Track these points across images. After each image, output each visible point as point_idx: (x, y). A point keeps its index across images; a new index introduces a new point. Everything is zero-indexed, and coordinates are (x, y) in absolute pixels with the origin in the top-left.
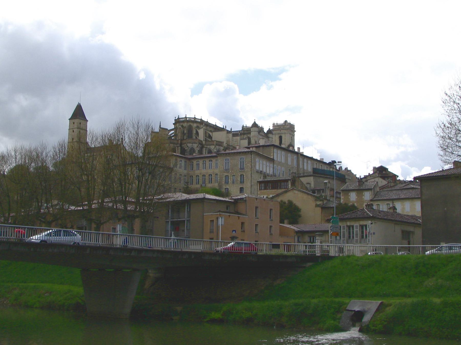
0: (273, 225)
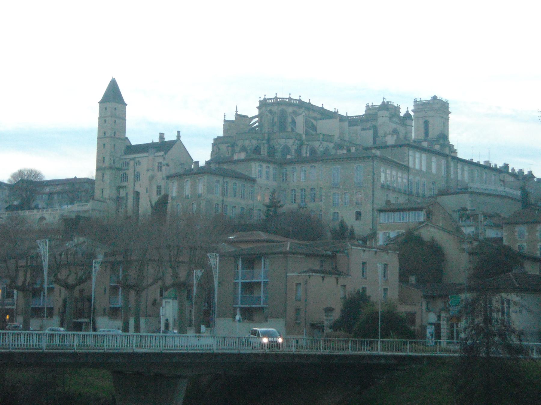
0: (388, 287)
